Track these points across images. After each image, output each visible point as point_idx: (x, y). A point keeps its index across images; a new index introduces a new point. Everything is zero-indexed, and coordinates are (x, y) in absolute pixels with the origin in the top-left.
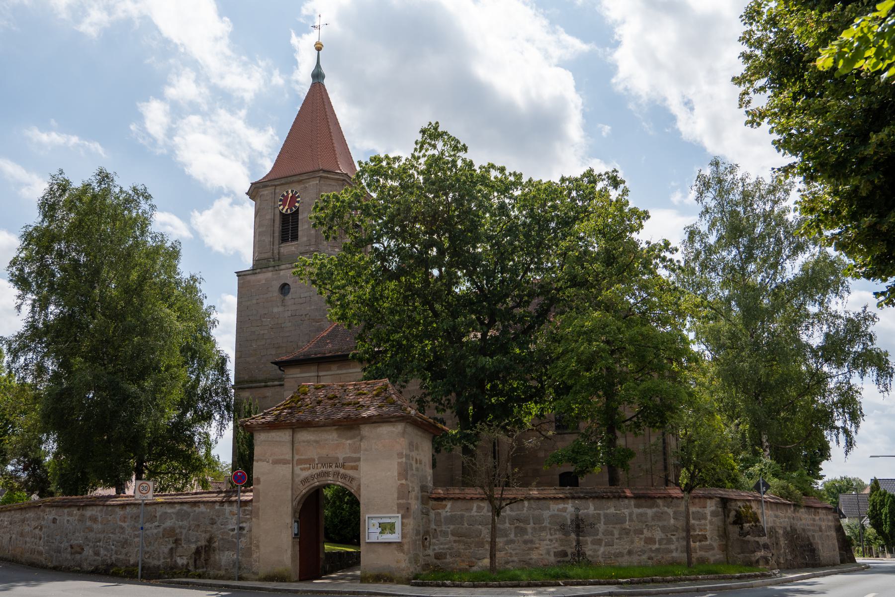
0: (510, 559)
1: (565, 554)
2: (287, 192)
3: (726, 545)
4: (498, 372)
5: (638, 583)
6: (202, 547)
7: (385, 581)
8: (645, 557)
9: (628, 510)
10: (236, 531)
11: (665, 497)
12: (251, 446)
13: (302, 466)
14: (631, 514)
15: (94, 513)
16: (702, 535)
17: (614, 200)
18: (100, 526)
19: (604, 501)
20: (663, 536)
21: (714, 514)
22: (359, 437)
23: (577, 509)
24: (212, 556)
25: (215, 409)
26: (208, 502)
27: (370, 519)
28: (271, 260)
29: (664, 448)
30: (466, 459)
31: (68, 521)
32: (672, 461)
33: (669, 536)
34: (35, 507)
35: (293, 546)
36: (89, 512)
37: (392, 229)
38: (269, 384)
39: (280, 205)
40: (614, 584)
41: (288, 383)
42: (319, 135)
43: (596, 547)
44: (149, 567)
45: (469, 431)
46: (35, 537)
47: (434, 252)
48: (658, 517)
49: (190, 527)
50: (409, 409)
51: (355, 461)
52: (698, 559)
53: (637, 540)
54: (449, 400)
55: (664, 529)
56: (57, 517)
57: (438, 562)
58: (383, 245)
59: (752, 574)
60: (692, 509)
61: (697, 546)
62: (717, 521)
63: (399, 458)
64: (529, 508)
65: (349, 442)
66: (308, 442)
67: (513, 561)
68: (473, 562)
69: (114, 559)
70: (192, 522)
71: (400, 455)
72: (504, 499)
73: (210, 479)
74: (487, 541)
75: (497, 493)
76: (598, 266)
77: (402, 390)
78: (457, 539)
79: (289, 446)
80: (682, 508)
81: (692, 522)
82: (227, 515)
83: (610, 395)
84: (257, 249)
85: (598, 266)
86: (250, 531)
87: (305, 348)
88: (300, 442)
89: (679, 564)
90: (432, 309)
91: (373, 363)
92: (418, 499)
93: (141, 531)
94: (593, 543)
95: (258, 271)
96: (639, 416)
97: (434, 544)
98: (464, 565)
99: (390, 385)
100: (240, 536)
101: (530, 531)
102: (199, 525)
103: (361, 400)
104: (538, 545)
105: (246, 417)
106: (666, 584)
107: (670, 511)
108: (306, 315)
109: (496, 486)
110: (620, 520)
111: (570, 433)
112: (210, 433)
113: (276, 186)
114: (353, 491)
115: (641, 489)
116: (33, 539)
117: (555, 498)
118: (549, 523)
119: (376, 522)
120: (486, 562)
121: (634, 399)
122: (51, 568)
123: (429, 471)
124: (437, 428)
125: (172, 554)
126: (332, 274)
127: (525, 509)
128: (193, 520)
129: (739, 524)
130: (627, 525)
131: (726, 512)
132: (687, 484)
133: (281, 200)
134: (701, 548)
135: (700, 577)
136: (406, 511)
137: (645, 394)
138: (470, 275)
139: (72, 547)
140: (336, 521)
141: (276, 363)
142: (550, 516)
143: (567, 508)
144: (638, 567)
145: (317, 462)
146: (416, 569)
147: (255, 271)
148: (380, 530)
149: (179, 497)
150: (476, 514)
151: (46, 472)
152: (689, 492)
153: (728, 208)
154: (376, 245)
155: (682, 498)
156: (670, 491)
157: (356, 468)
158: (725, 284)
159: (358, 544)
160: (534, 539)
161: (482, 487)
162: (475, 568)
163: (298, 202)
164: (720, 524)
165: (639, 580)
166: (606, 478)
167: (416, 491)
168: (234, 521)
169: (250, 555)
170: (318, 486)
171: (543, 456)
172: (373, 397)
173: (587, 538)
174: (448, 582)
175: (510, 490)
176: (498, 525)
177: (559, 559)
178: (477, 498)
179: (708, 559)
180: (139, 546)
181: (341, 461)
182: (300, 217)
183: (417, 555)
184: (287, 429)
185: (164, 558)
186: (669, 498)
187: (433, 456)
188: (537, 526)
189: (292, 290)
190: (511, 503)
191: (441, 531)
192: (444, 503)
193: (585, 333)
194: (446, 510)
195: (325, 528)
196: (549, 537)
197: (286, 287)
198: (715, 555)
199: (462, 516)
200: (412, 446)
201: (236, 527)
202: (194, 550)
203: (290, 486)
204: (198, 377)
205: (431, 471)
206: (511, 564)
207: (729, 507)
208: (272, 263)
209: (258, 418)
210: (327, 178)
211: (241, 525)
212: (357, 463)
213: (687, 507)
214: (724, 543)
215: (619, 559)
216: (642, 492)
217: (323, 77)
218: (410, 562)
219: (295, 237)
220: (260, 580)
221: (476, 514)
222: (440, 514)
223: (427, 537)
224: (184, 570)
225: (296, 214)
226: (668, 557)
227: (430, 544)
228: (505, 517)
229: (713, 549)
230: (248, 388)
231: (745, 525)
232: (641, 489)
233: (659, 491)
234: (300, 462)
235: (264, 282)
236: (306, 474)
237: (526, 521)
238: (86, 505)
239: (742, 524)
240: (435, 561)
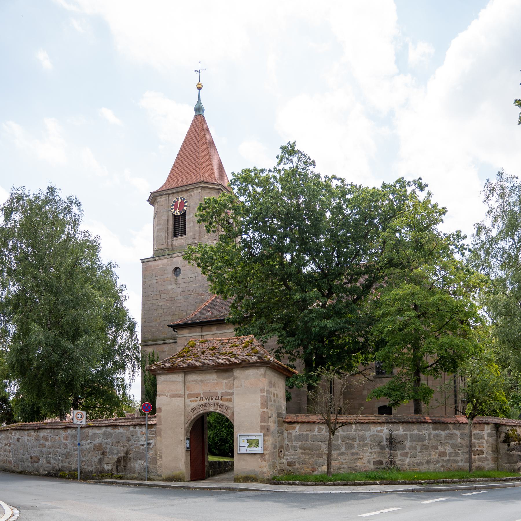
0: (342, 466)
1: (381, 463)
2: (178, 199)
3: (497, 458)
4: (335, 331)
5: (433, 483)
6: (121, 457)
7: (252, 481)
8: (438, 465)
9: (427, 431)
10: (145, 446)
11: (454, 423)
12: (154, 385)
13: (192, 399)
14: (429, 435)
15: (45, 434)
16: (480, 450)
17: (422, 201)
18: (50, 443)
19: (410, 425)
20: (452, 450)
21: (489, 435)
22: (233, 378)
23: (391, 431)
24: (128, 464)
25: (128, 360)
26: (125, 425)
27: (241, 437)
28: (167, 250)
29: (455, 387)
30: (310, 393)
31: (28, 440)
32: (461, 397)
33: (456, 450)
34: (5, 430)
35: (186, 456)
36: (42, 434)
37: (257, 224)
38: (166, 341)
39: (172, 209)
40: (416, 484)
41: (179, 341)
42: (200, 155)
44: (85, 472)
45: (313, 373)
46: (6, 451)
47: (288, 241)
48: (449, 437)
49: (113, 443)
50: (269, 357)
51: (230, 395)
52: (477, 467)
53: (433, 453)
54: (298, 352)
55: (453, 446)
56: (20, 437)
57: (290, 468)
58: (249, 236)
59: (515, 477)
60: (474, 432)
61: (477, 458)
62: (492, 440)
63: (261, 393)
64: (356, 430)
65: (225, 381)
66: (196, 381)
67: (343, 468)
68: (315, 468)
69: (60, 466)
70: (114, 440)
71: (262, 390)
72: (337, 423)
73: (125, 412)
74: (325, 453)
75: (333, 418)
76: (409, 252)
77: (264, 344)
78: (303, 451)
79: (182, 384)
80: (467, 431)
81: (473, 440)
82: (139, 434)
83: (416, 347)
84: (156, 242)
85: (409, 252)
86: (155, 445)
87: (192, 315)
88: (189, 382)
89: (463, 470)
90: (286, 284)
91: (242, 325)
92: (275, 423)
93: (78, 447)
94: (401, 455)
95: (157, 258)
96: (438, 363)
97: (287, 455)
98: (308, 471)
99: (254, 340)
100: (148, 449)
101: (356, 446)
102: (119, 442)
103: (233, 350)
104: (361, 457)
105: (150, 364)
106: (454, 484)
107: (458, 433)
108: (192, 291)
109: (332, 413)
110: (420, 439)
111: (386, 377)
112: (125, 378)
113: (169, 194)
114: (228, 416)
115: (438, 417)
116: (5, 453)
117: (375, 423)
118: (370, 441)
119: (245, 439)
120: (325, 468)
121: (433, 350)
122: (18, 473)
123: (283, 403)
124: (289, 371)
125: (101, 462)
126: (212, 259)
128: (115, 438)
129: (507, 442)
130: (426, 442)
131: (498, 434)
132: (471, 413)
133: (173, 205)
134: (479, 460)
135: (478, 479)
136: (266, 430)
137: (441, 347)
138: (313, 258)
139: (31, 458)
140: (217, 439)
141: (171, 326)
142: (371, 436)
143: (383, 430)
144: (434, 472)
145: (202, 396)
146: (274, 473)
147: (154, 259)
148: (248, 444)
149: (104, 422)
150: (317, 433)
151: (10, 406)
152: (472, 419)
153: (507, 208)
154: (244, 237)
155: (467, 423)
156: (458, 419)
157: (230, 400)
158: (502, 267)
159: (233, 456)
160: (359, 452)
161: (322, 414)
162: (316, 473)
163: (186, 206)
164: (494, 442)
165: (434, 482)
166: (412, 409)
167: (274, 417)
168: (143, 438)
169: (156, 463)
170: (203, 413)
171: (366, 394)
172: (243, 348)
173: (398, 451)
174: (297, 482)
175: (342, 416)
176: (333, 442)
177: (377, 466)
178: (318, 422)
179: (484, 467)
180: (77, 457)
181: (219, 395)
182: (187, 217)
183: (274, 463)
184: (180, 372)
185: (95, 465)
186: (457, 424)
187: (287, 391)
188: (361, 443)
189: (182, 272)
190: (343, 425)
191: (292, 446)
192: (294, 425)
193: (399, 299)
194: (296, 431)
195: (209, 445)
196: (370, 450)
197: (178, 270)
198: (489, 464)
199: (307, 435)
200: (271, 384)
201: (145, 443)
202: (116, 460)
204: (115, 337)
205: (285, 403)
206: (342, 469)
207: (500, 431)
208: (167, 252)
209: (159, 365)
210: (207, 188)
211: (149, 442)
212: (231, 397)
213: (470, 430)
214: (496, 456)
215: (420, 467)
216: (438, 419)
217: (203, 111)
218: (270, 468)
219: (184, 233)
220: (163, 480)
221: (317, 433)
222: (291, 433)
223: (282, 450)
224: (110, 474)
225: (184, 215)
226: (455, 466)
227: (284, 455)
228: (338, 436)
229: (488, 460)
230: (151, 345)
231: (511, 443)
232: (438, 417)
233: (450, 419)
234: (190, 396)
235: (161, 266)
236: (194, 404)
237: (354, 439)
238: (40, 429)
239: (509, 443)
240: (288, 467)
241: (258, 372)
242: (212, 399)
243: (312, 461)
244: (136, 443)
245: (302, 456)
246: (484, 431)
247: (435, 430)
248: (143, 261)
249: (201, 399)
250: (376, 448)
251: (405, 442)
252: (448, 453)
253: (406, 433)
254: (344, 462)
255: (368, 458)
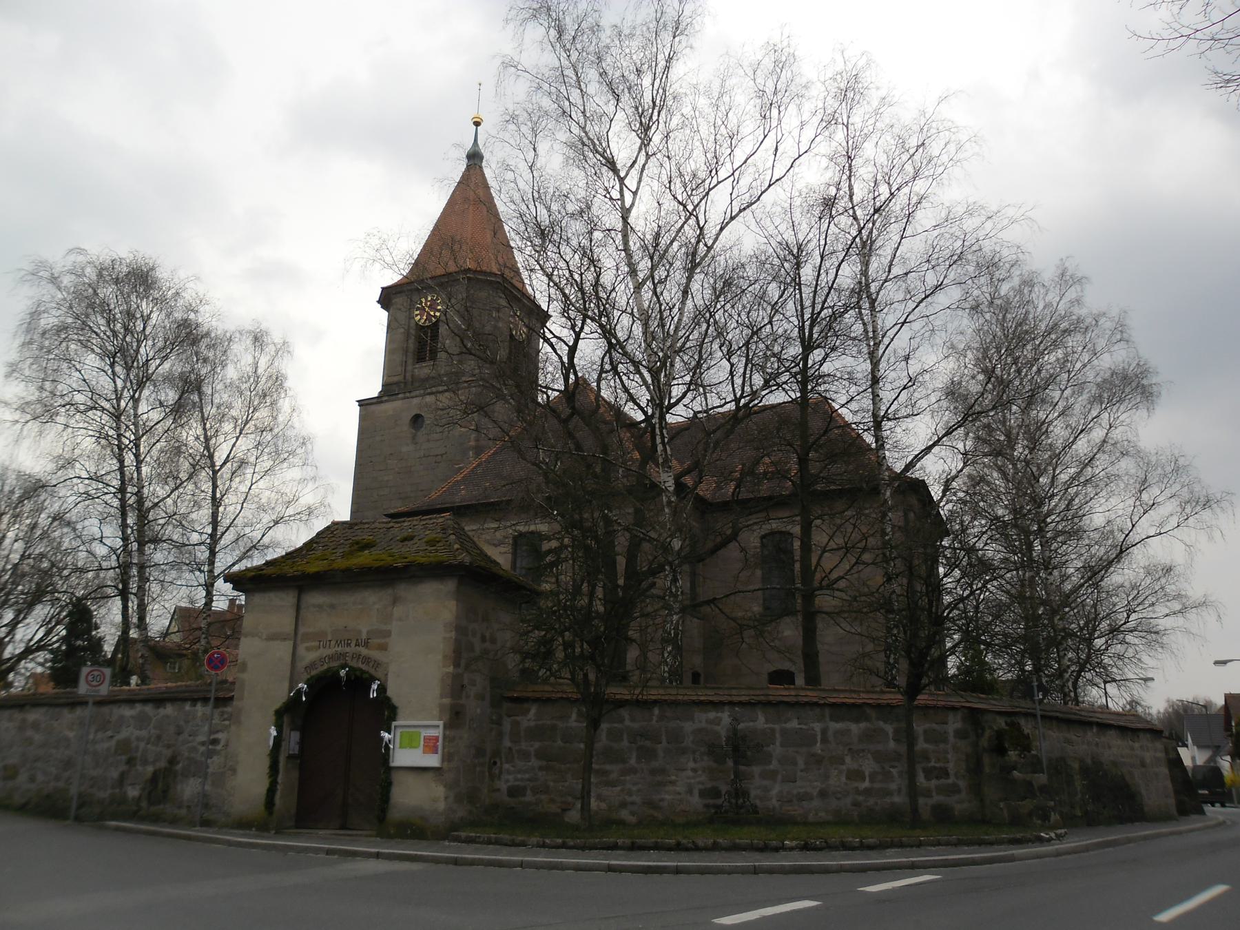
0: (629, 799)
1: (715, 793)
5: (871, 848)
14: (824, 732)
16: (941, 768)
21: (960, 734)
23: (736, 720)
39: (417, 315)
43: (766, 783)
66: (320, 607)
67: (633, 803)
70: (153, 731)
78: (544, 763)
79: (292, 612)
86: (226, 745)
92: (483, 698)
98: (554, 808)
100: (210, 754)
127: (655, 718)
130: (818, 748)
181: (364, 636)
192: (526, 705)
194: (529, 717)
196: (691, 765)
197: (420, 420)
203: (288, 674)
223: (498, 760)
227: (501, 773)
241: (442, 587)
242: (349, 645)
243: (563, 786)
244: (191, 738)
245: (540, 774)
246: (946, 723)
247: (837, 721)
248: (362, 403)
249: (328, 643)
250: (705, 758)
251: (768, 746)
252: (867, 774)
253: (772, 726)
254: (634, 788)
255: (688, 781)
